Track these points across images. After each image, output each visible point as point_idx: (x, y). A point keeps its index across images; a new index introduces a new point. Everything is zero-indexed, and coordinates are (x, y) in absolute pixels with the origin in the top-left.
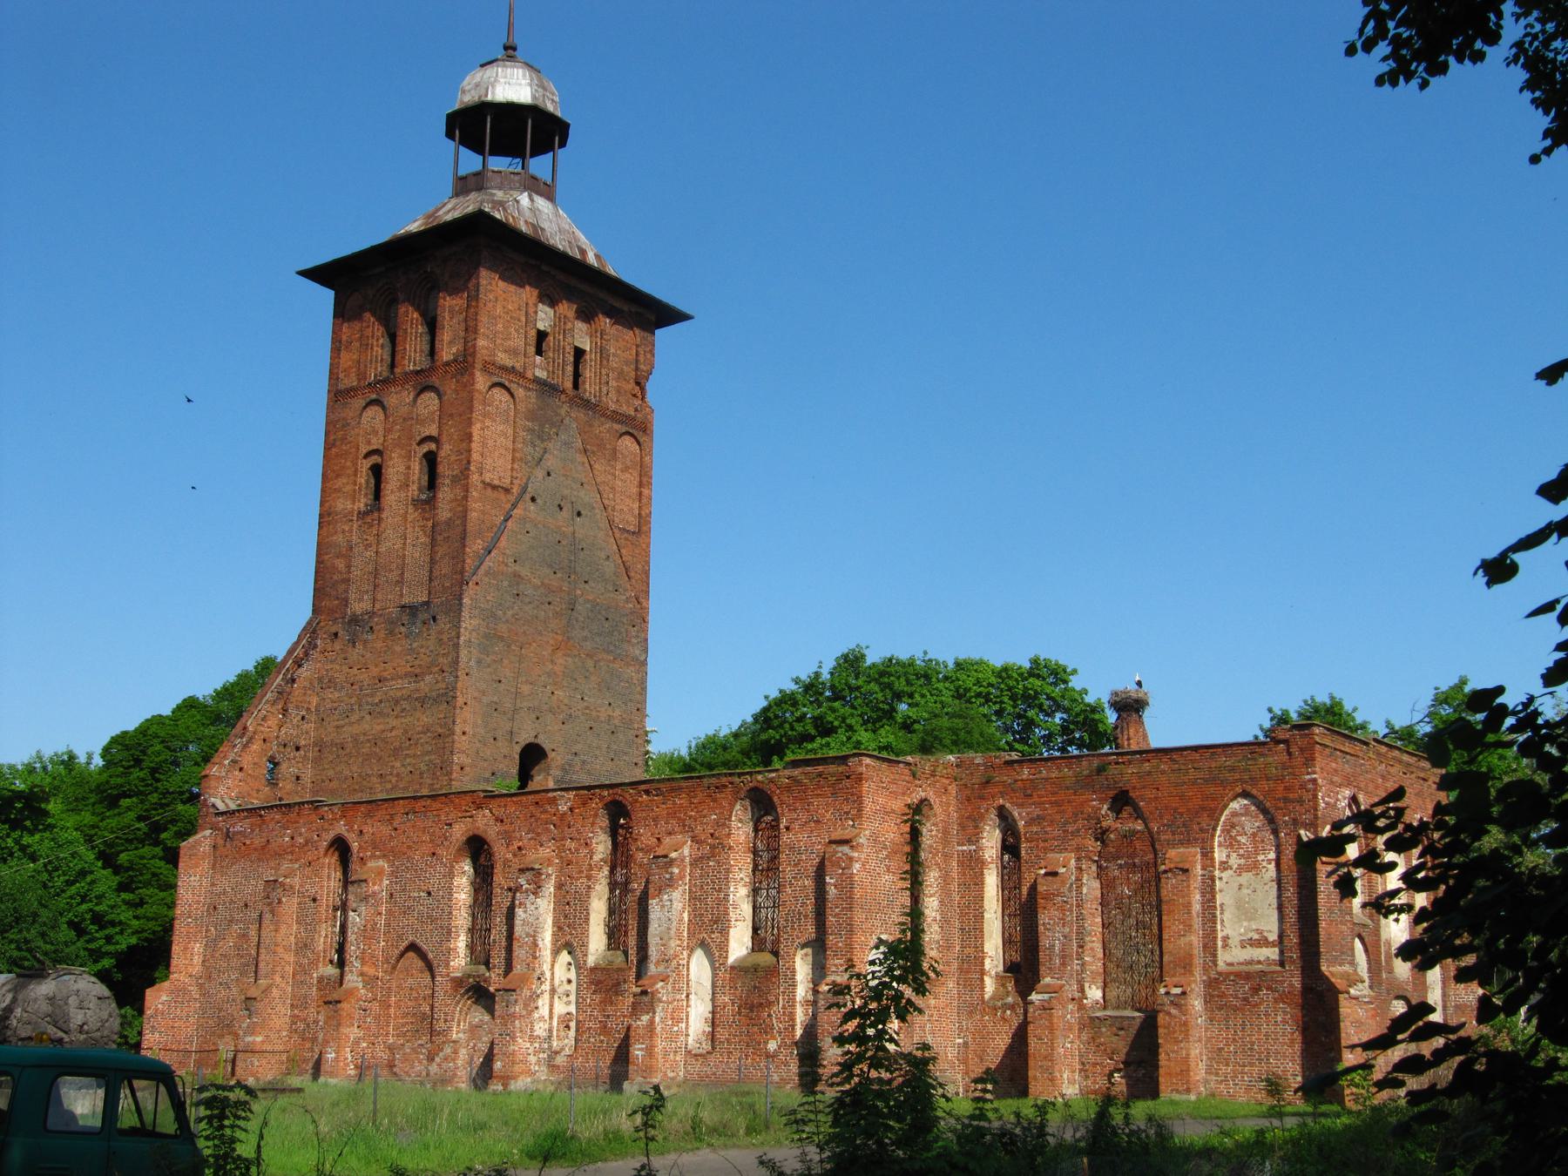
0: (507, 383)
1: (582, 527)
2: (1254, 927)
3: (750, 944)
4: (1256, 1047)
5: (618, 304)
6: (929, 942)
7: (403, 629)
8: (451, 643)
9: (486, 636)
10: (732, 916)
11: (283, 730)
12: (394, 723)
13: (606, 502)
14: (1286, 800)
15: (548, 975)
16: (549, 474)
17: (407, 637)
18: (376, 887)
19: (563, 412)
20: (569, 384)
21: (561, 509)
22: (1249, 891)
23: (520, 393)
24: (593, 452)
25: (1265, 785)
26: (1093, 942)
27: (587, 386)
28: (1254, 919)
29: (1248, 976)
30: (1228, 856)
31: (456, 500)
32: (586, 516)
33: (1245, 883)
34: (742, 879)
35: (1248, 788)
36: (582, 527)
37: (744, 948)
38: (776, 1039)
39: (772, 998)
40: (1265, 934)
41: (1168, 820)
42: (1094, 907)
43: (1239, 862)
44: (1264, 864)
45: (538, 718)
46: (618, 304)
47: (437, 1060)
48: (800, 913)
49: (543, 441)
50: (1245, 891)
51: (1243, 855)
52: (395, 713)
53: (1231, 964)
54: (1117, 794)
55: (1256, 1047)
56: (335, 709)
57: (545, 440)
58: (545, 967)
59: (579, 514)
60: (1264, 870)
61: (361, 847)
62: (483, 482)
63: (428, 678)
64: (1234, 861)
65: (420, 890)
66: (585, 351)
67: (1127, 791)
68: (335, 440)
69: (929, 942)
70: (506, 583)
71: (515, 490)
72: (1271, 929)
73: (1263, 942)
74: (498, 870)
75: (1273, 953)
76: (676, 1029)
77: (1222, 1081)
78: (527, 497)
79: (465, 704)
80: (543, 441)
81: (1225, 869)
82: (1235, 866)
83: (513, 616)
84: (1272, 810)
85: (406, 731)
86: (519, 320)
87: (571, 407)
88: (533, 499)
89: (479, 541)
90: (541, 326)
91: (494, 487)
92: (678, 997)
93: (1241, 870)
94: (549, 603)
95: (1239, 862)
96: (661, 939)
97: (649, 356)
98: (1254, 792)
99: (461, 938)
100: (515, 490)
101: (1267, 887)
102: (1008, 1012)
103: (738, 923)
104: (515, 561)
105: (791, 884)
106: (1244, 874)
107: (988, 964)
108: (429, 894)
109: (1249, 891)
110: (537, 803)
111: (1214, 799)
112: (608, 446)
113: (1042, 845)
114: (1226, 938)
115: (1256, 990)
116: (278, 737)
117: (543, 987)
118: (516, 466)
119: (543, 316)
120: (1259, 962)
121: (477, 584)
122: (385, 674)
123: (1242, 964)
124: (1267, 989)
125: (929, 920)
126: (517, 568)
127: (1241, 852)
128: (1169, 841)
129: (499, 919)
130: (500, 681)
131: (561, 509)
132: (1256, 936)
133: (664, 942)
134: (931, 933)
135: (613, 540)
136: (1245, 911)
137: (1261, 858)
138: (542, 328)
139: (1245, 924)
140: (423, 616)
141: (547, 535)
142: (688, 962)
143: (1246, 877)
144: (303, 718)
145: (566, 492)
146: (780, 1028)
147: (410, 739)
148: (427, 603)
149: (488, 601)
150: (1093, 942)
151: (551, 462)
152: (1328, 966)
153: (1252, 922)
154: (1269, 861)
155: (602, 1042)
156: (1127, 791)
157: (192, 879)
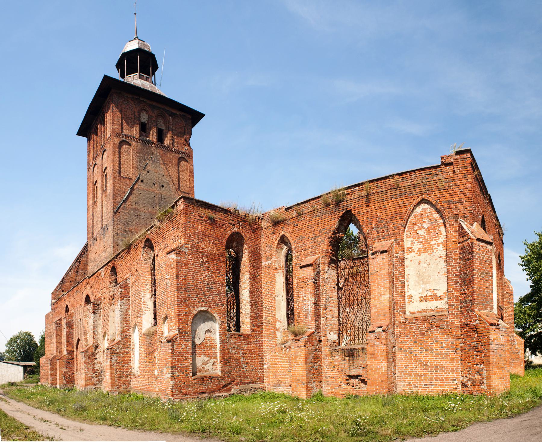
1: (164, 191)
2: (429, 288)
4: (429, 364)
6: (245, 314)
9: (125, 231)
10: (143, 308)
11: (77, 278)
14: (451, 202)
19: (153, 150)
21: (155, 185)
22: (425, 265)
24: (167, 164)
25: (437, 194)
26: (332, 307)
28: (429, 283)
29: (424, 319)
30: (412, 243)
32: (166, 187)
33: (423, 260)
34: (148, 289)
35: (426, 197)
36: (164, 191)
37: (150, 324)
40: (435, 292)
41: (375, 224)
42: (333, 286)
43: (419, 246)
44: (436, 246)
46: (175, 112)
49: (145, 160)
50: (422, 265)
51: (421, 242)
53: (414, 313)
54: (344, 214)
55: (429, 364)
57: (146, 160)
59: (163, 186)
60: (435, 251)
64: (416, 246)
66: (163, 130)
67: (350, 211)
69: (245, 314)
70: (132, 212)
72: (442, 287)
73: (434, 297)
75: (442, 304)
76: (126, 365)
77: (407, 385)
78: (140, 180)
80: (145, 160)
81: (411, 252)
82: (416, 250)
83: (136, 223)
84: (442, 210)
87: (156, 148)
88: (142, 181)
93: (420, 252)
94: (152, 218)
95: (419, 246)
97: (189, 130)
98: (430, 199)
101: (437, 262)
102: (288, 350)
103: (146, 312)
106: (422, 254)
107: (278, 325)
109: (425, 265)
111: (403, 207)
112: (174, 162)
113: (303, 252)
114: (410, 297)
115: (430, 328)
116: (75, 280)
120: (431, 310)
123: (420, 312)
124: (437, 327)
125: (244, 302)
126: (137, 206)
127: (421, 240)
128: (375, 238)
131: (155, 185)
132: (429, 294)
134: (246, 309)
136: (423, 279)
137: (432, 243)
139: (423, 286)
141: (149, 194)
143: (424, 256)
144: (85, 273)
145: (156, 178)
149: (124, 219)
150: (332, 307)
151: (149, 168)
152: (479, 309)
153: (428, 285)
154: (439, 245)
156: (350, 211)
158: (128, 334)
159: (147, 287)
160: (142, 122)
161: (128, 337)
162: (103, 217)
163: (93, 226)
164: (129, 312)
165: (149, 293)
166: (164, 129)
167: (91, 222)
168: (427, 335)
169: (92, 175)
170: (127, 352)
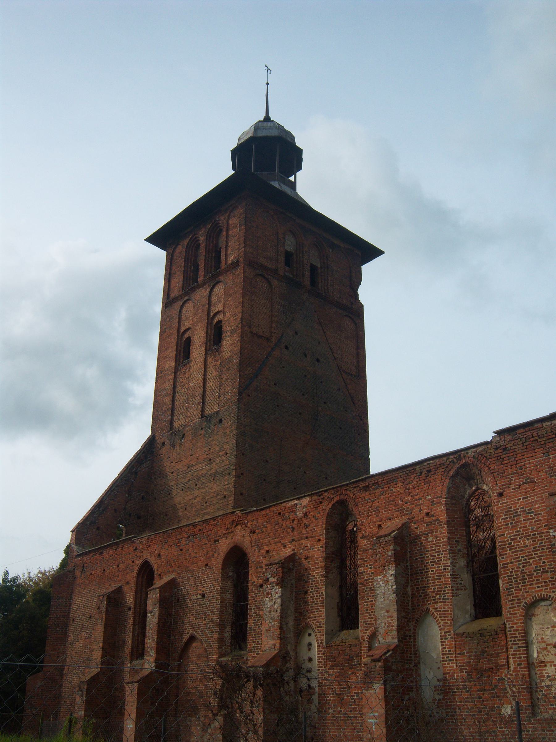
0: (266, 275)
3: (473, 612)
5: (336, 242)
7: (203, 432)
8: (231, 434)
12: (196, 493)
13: (336, 356)
15: (292, 654)
16: (296, 333)
17: (204, 436)
18: (167, 594)
20: (307, 282)
21: (306, 356)
23: (275, 282)
27: (320, 287)
31: (234, 343)
34: (460, 550)
37: (467, 616)
38: (511, 703)
39: (502, 661)
45: (295, 489)
46: (336, 242)
47: (209, 730)
48: (523, 573)
52: (198, 486)
56: (163, 491)
58: (289, 648)
59: (318, 361)
61: (158, 567)
62: (251, 332)
63: (218, 460)
65: (197, 594)
68: (165, 328)
71: (274, 340)
74: (252, 571)
79: (242, 474)
85: (204, 498)
86: (273, 241)
88: (286, 347)
89: (249, 369)
90: (288, 248)
91: (260, 337)
92: (407, 666)
94: (300, 414)
96: (388, 611)
99: (227, 630)
100: (274, 340)
103: (460, 592)
104: (275, 384)
105: (511, 547)
108: (203, 596)
110: (280, 513)
116: (125, 509)
117: (288, 665)
118: (274, 325)
119: (289, 243)
121: (249, 396)
122: (192, 463)
129: (253, 611)
130: (267, 461)
133: (390, 614)
135: (341, 379)
138: (289, 250)
140: (215, 420)
142: (414, 633)
144: (143, 498)
146: (514, 692)
147: (206, 503)
148: (217, 413)
155: (339, 712)
157: (60, 600)
158: (407, 633)
159: (459, 547)
160: (286, 251)
161: (408, 638)
162: (177, 397)
163: (173, 409)
164: (407, 590)
165: (463, 557)
166: (319, 266)
167: (168, 400)
168: (459, 715)
169: (176, 317)
170: (407, 669)
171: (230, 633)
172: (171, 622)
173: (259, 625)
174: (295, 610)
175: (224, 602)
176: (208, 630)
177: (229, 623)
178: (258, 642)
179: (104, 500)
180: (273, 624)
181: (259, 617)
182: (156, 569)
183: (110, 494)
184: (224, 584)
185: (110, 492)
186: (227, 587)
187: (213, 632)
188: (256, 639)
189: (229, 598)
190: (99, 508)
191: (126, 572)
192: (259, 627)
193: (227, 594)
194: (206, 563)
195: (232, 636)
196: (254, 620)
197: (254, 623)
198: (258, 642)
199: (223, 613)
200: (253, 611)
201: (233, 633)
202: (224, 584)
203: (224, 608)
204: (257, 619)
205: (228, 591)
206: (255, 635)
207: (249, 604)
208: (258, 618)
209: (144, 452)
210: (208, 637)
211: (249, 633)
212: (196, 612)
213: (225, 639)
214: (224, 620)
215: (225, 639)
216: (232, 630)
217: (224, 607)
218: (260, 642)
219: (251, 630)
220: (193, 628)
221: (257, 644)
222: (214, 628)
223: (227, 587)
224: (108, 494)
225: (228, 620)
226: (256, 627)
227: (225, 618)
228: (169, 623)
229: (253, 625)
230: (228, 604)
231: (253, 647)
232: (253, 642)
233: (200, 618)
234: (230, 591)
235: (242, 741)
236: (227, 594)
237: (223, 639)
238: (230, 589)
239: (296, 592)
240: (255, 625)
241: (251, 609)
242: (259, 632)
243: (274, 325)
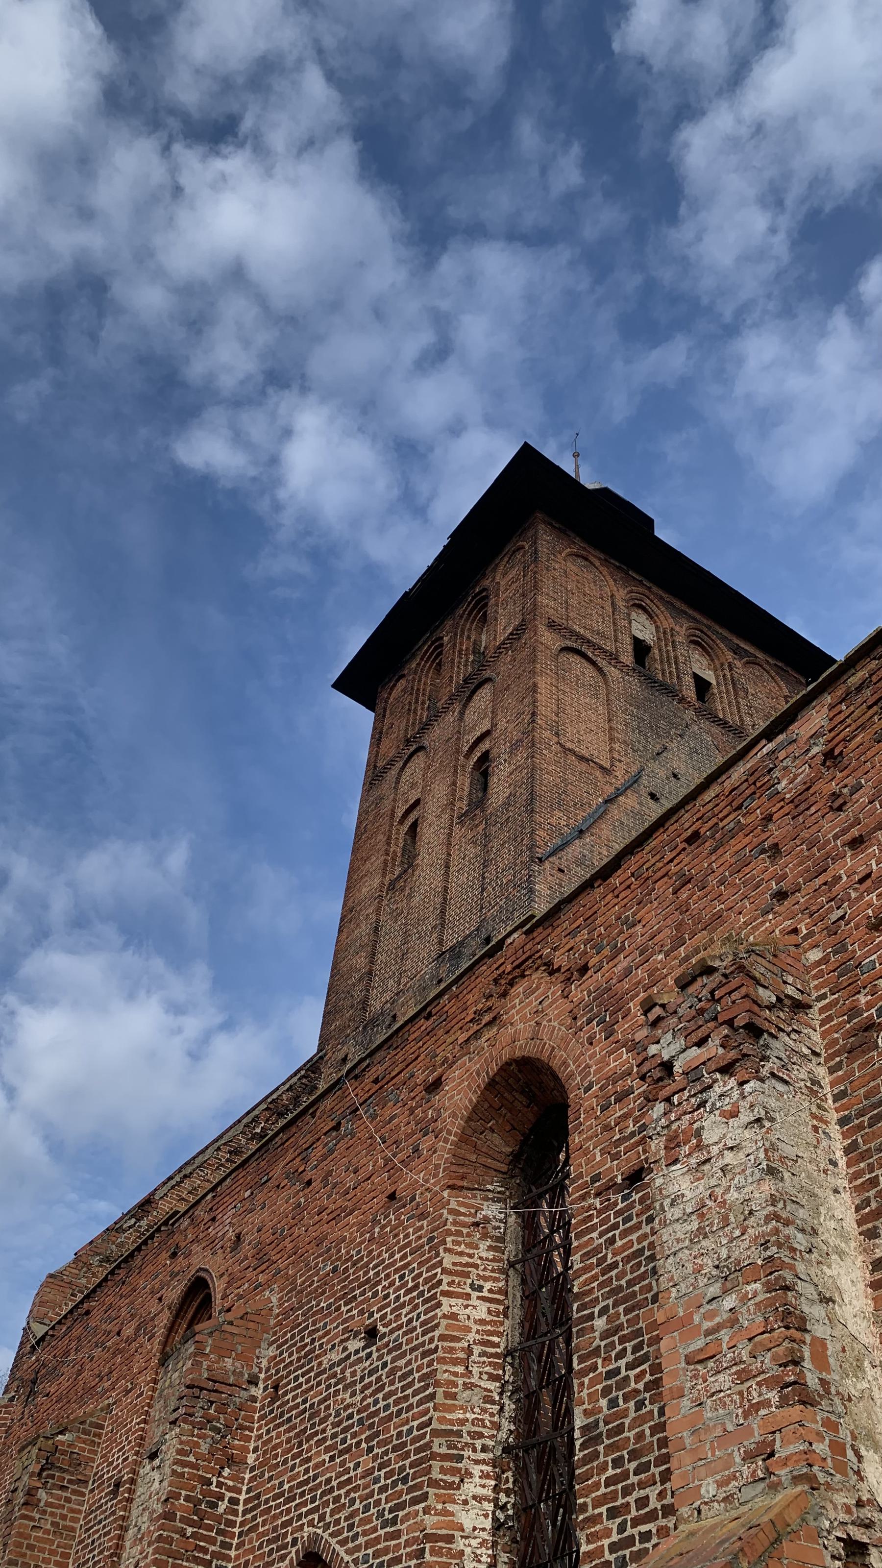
23: (613, 672)
99: (471, 1488)
166: (714, 682)
167: (361, 961)
171: (489, 1507)
172: (234, 1501)
173: (637, 1391)
174: (860, 1223)
175: (458, 1339)
176: (378, 1503)
177: (484, 1449)
178: (642, 1502)
179: (157, 1197)
180: (729, 1302)
181: (636, 1349)
182: (219, 1296)
183: (178, 1184)
184: (461, 1254)
185: (177, 1179)
186: (476, 1266)
187: (401, 1506)
188: (627, 1491)
189: (482, 1322)
190: (138, 1220)
191: (135, 1345)
192: (640, 1405)
193: (474, 1301)
194: (391, 1189)
195: (498, 1526)
196: (610, 1374)
197: (606, 1391)
198: (642, 1502)
199: (454, 1396)
200: (600, 1323)
201: (503, 1508)
202: (461, 1254)
203: (460, 1369)
204: (622, 1363)
205: (480, 1288)
206: (618, 1462)
207: (578, 1296)
208: (630, 1357)
209: (290, 1089)
210: (377, 1540)
211: (586, 1460)
212: (335, 1425)
213: (460, 1544)
214: (459, 1434)
215: (460, 1544)
216: (496, 1489)
217: (455, 1362)
218: (654, 1503)
219: (597, 1439)
220: (315, 1510)
221: (636, 1522)
222: (405, 1480)
223: (476, 1266)
224: (173, 1182)
225: (481, 1435)
226: (625, 1413)
227: (463, 1422)
228: (222, 1506)
229: (603, 1403)
230: (477, 1349)
231: (613, 1548)
232: (613, 1513)
233: (348, 1450)
234: (488, 1285)
235: (745, 1564)
236: (474, 1301)
237: (450, 1539)
238: (486, 1279)
239: (842, 1122)
240: (613, 1403)
241: (591, 1317)
242: (640, 1436)
243: (616, 746)
